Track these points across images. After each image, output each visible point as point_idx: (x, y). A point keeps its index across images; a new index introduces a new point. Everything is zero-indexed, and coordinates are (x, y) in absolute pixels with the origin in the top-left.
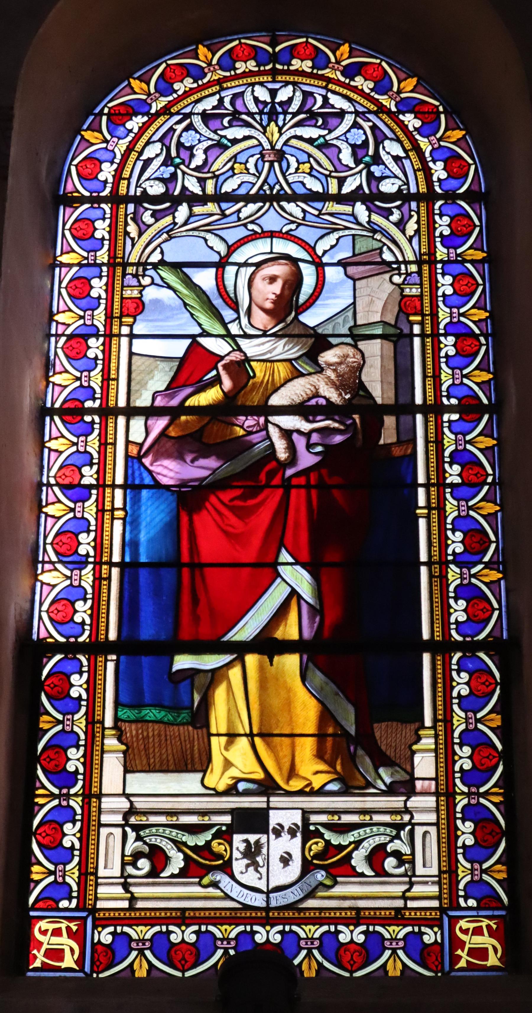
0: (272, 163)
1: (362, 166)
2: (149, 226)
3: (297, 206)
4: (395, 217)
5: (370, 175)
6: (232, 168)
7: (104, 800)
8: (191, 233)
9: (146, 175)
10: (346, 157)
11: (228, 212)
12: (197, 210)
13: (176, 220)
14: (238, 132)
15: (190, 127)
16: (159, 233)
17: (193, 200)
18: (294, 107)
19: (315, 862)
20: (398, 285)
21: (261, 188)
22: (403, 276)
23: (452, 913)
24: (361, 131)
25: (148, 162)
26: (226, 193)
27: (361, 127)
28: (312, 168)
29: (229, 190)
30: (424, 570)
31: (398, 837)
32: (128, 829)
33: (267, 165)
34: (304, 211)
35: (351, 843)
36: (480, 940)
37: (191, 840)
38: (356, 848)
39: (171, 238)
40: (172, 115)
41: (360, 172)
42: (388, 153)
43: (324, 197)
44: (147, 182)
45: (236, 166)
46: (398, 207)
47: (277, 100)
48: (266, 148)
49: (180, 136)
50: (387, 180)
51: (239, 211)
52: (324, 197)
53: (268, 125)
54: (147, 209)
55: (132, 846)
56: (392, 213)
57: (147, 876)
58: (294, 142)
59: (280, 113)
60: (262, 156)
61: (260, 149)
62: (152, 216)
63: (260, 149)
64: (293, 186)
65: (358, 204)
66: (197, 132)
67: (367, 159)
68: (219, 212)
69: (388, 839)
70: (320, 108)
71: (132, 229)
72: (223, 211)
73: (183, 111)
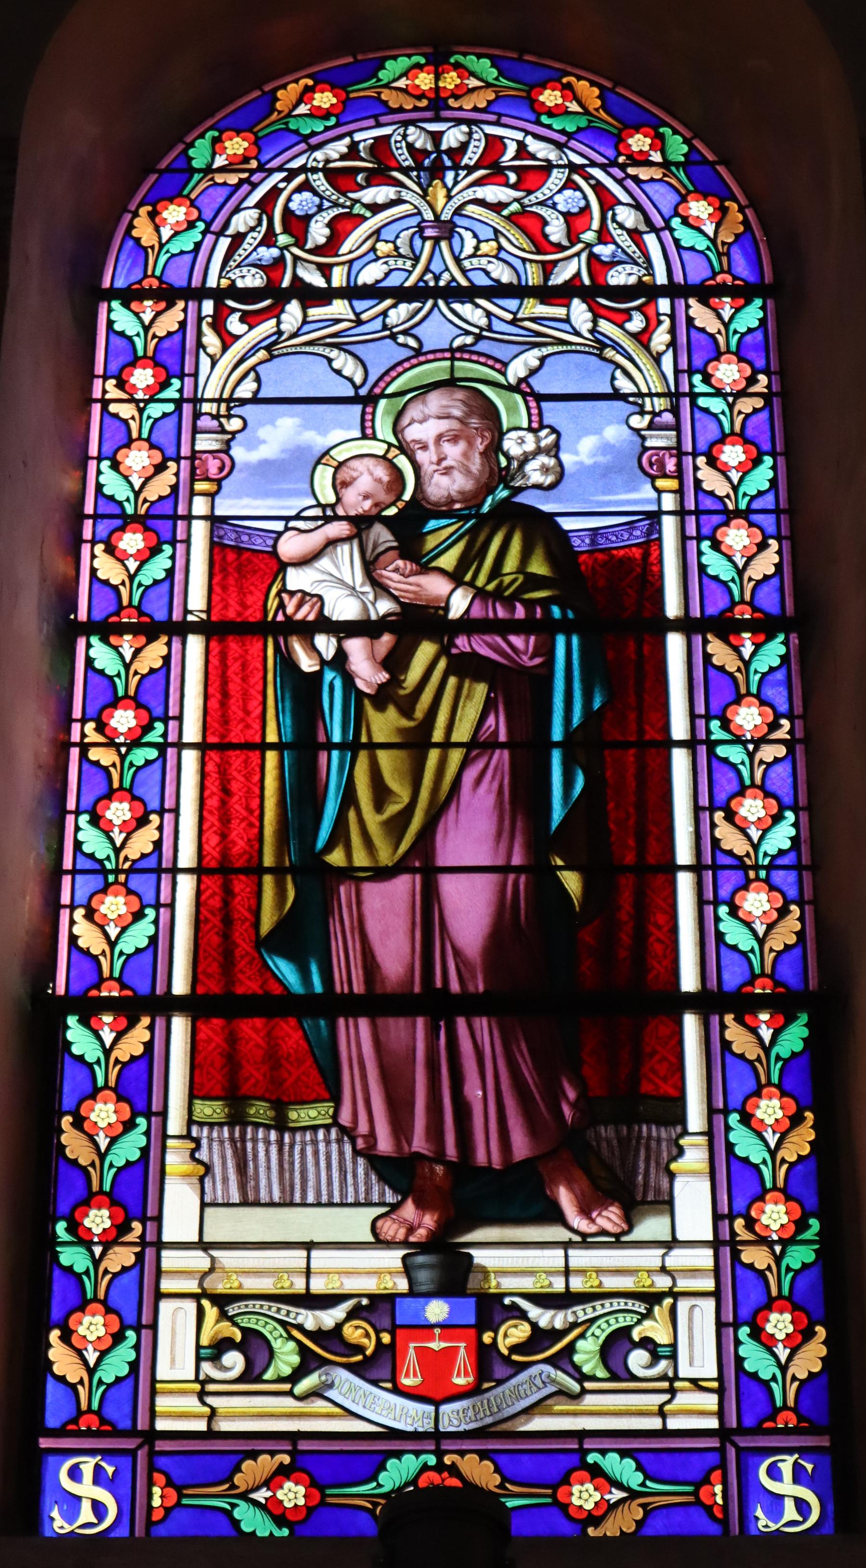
0: (437, 241)
1: (579, 246)
2: (237, 338)
3: (478, 306)
4: (636, 323)
5: (593, 258)
6: (373, 249)
7: (165, 1253)
8: (304, 349)
11: (364, 317)
12: (315, 313)
13: (283, 327)
14: (381, 194)
15: (306, 186)
16: (254, 349)
17: (311, 297)
18: (471, 157)
19: (515, 1357)
20: (637, 431)
21: (421, 279)
23: (744, 1442)
24: (578, 194)
25: (238, 239)
26: (365, 285)
27: (577, 188)
28: (500, 248)
29: (370, 281)
30: (685, 883)
32: (206, 1303)
33: (428, 245)
34: (489, 314)
35: (574, 1325)
37: (309, 1319)
39: (272, 357)
40: (271, 172)
41: (578, 254)
43: (518, 291)
44: (237, 271)
45: (379, 245)
47: (444, 147)
48: (426, 217)
49: (289, 200)
50: (619, 268)
51: (384, 314)
52: (518, 291)
53: (430, 185)
54: (234, 310)
55: (213, 1327)
56: (630, 319)
57: (239, 1380)
58: (471, 209)
59: (449, 168)
60: (421, 229)
61: (418, 219)
63: (418, 219)
64: (470, 274)
65: (576, 302)
66: (315, 193)
68: (352, 317)
69: (636, 1317)
70: (513, 159)
71: (211, 340)
72: (357, 315)
73: (288, 166)
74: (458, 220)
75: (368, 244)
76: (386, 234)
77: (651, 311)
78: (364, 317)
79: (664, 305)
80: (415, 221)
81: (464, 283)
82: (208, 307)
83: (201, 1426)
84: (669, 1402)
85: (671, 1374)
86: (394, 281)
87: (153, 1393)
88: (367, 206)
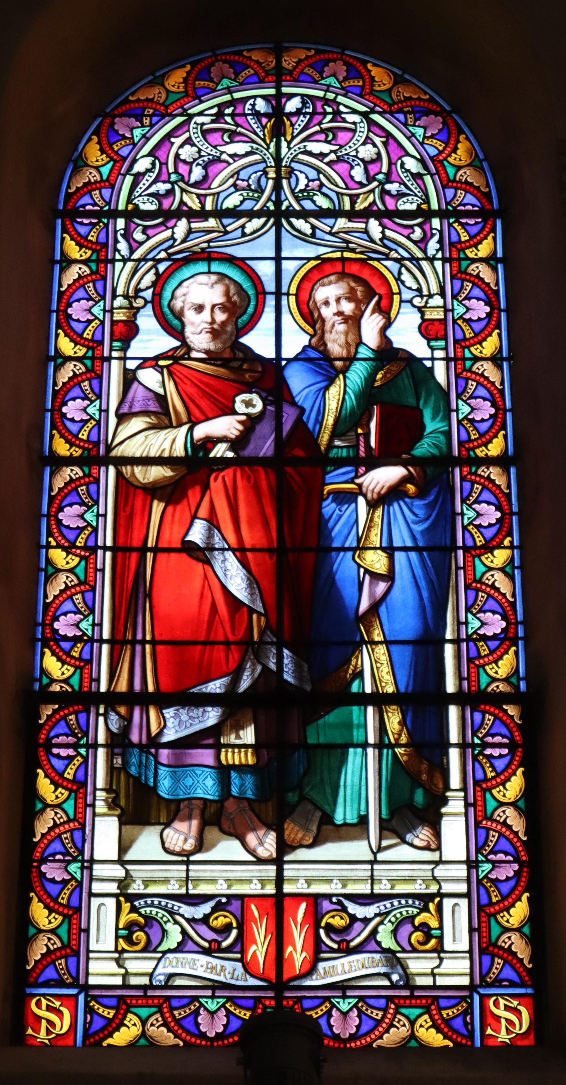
1: (375, 184)
2: (141, 244)
9: (139, 190)
10: (358, 173)
11: (229, 229)
13: (175, 236)
22: (425, 298)
23: (482, 991)
25: (138, 177)
28: (322, 185)
29: (231, 206)
31: (425, 909)
36: (510, 1020)
38: (381, 923)
41: (372, 191)
42: (407, 171)
46: (419, 225)
51: (243, 227)
61: (263, 165)
62: (144, 232)
63: (263, 165)
67: (381, 177)
71: (123, 246)
74: (293, 165)
75: (231, 181)
76: (243, 175)
77: (427, 227)
78: (229, 229)
79: (436, 223)
80: (262, 166)
81: (297, 207)
82: (121, 223)
83: (118, 981)
84: (438, 967)
85: (439, 949)
86: (248, 205)
87: (88, 959)
88: (231, 156)
